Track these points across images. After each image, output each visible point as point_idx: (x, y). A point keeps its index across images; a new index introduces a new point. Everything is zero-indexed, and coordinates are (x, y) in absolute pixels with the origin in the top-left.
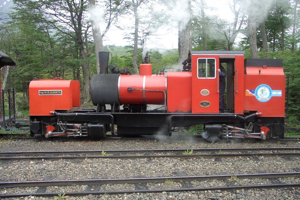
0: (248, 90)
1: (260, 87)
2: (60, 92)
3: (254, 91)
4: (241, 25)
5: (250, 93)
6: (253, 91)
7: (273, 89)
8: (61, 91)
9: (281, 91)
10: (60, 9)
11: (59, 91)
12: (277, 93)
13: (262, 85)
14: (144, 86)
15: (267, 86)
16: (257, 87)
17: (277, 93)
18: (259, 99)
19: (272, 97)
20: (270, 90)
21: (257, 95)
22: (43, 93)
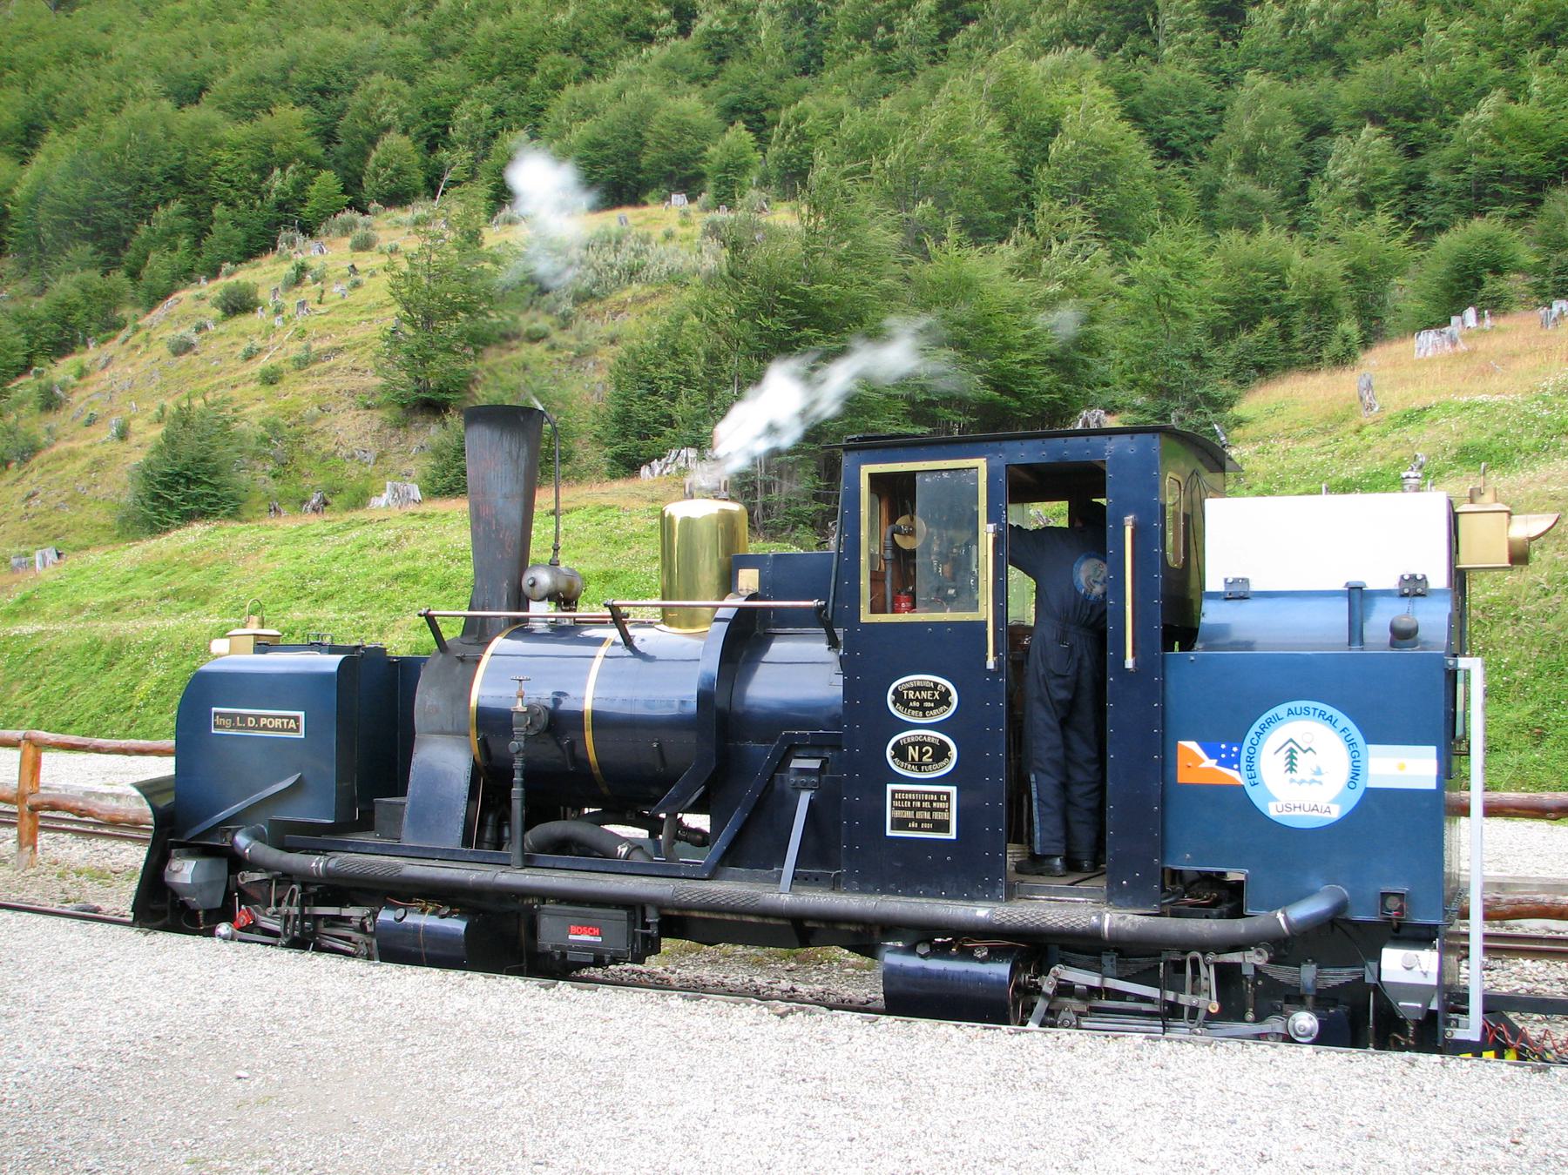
0: (1192, 746)
1: (1253, 746)
2: (292, 724)
3: (1238, 754)
4: (1116, 950)
5: (1211, 763)
6: (1228, 751)
7: (1370, 740)
8: (296, 719)
9: (1433, 750)
10: (1410, 1162)
11: (289, 718)
12: (1402, 767)
13: (1292, 705)
14: (1106, 926)
15: (1330, 711)
16: (1256, 727)
17: (1402, 767)
18: (1273, 811)
19: (1370, 793)
20: (1351, 744)
21: (1253, 778)
22: (228, 722)
